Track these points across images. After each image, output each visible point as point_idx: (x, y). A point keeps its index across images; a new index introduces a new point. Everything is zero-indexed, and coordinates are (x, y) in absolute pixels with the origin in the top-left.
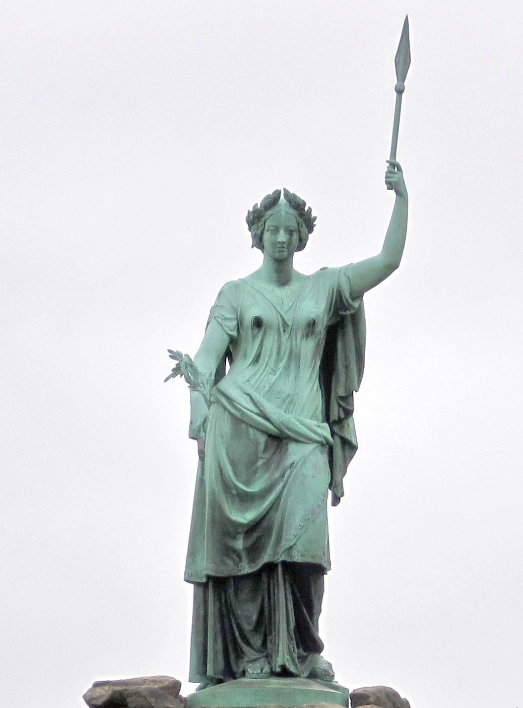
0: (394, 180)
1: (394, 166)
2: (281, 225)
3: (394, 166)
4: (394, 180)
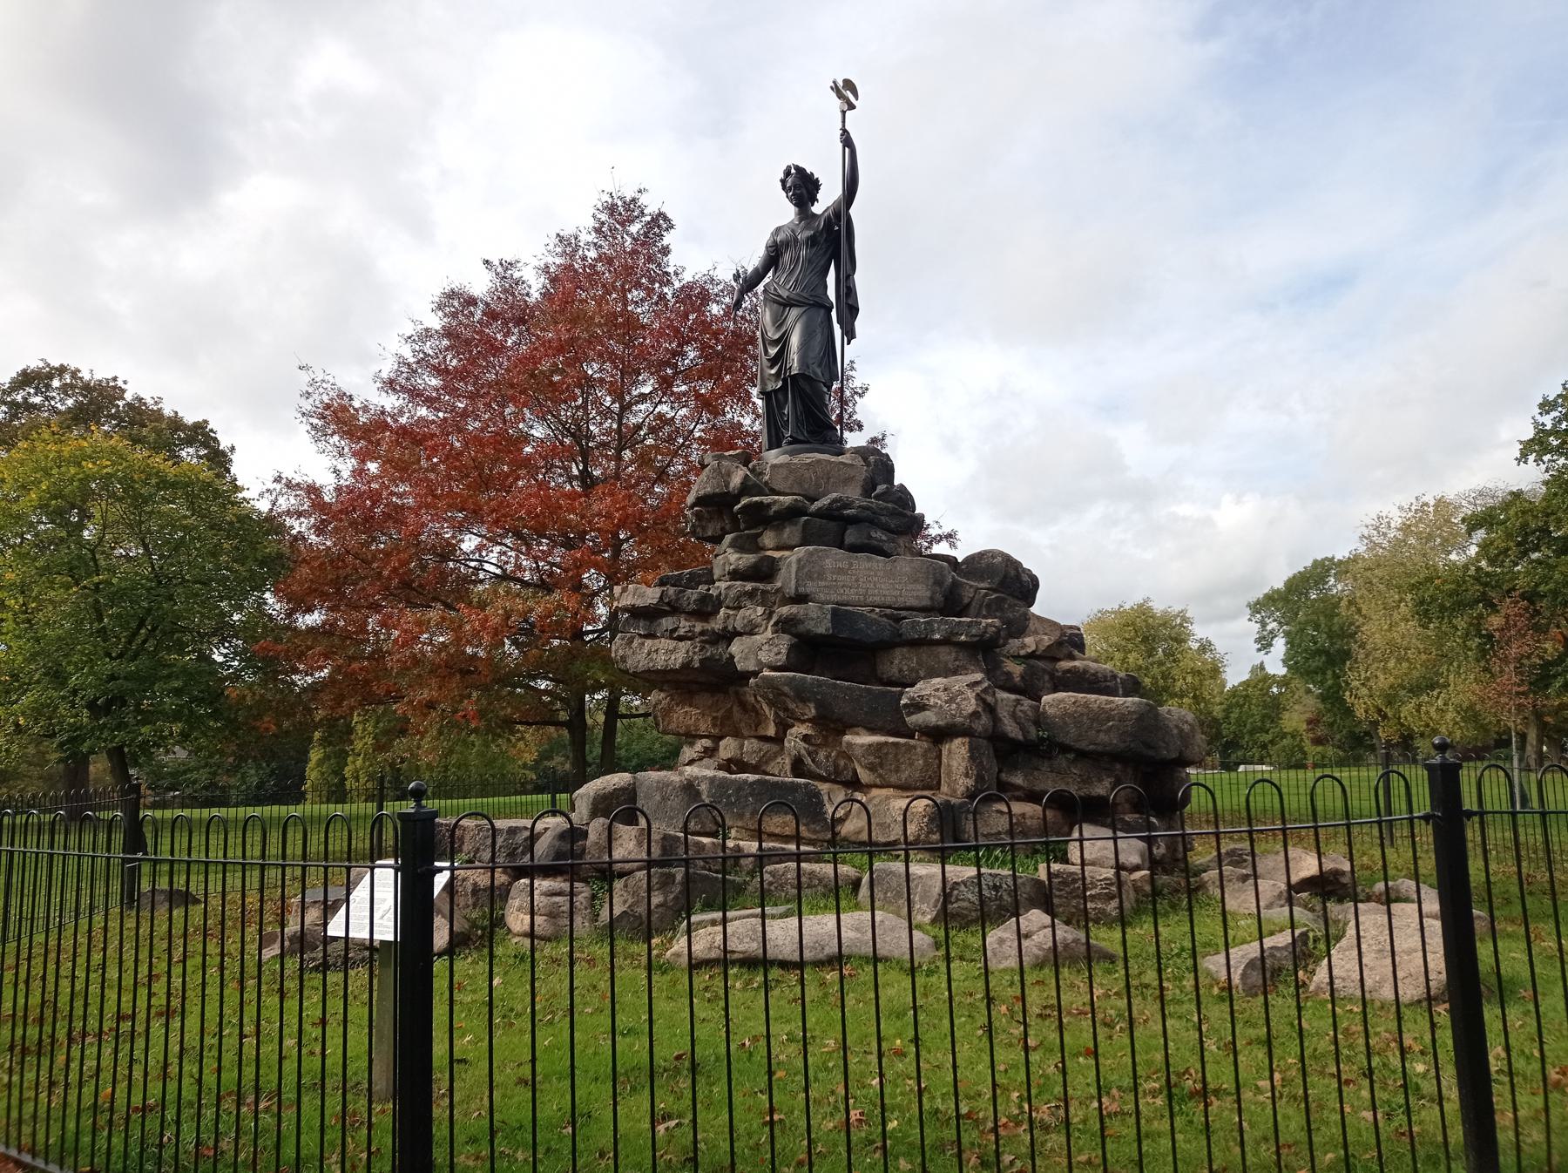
0: (847, 141)
1: (845, 131)
2: (801, 186)
3: (845, 131)
4: (847, 141)
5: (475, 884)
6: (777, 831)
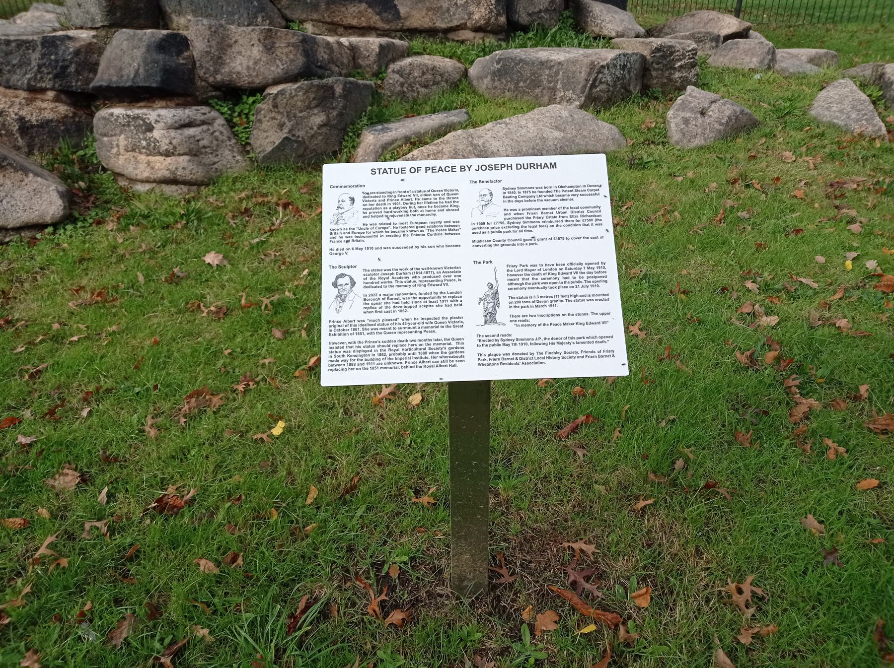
5: (21, 119)
6: (354, 22)
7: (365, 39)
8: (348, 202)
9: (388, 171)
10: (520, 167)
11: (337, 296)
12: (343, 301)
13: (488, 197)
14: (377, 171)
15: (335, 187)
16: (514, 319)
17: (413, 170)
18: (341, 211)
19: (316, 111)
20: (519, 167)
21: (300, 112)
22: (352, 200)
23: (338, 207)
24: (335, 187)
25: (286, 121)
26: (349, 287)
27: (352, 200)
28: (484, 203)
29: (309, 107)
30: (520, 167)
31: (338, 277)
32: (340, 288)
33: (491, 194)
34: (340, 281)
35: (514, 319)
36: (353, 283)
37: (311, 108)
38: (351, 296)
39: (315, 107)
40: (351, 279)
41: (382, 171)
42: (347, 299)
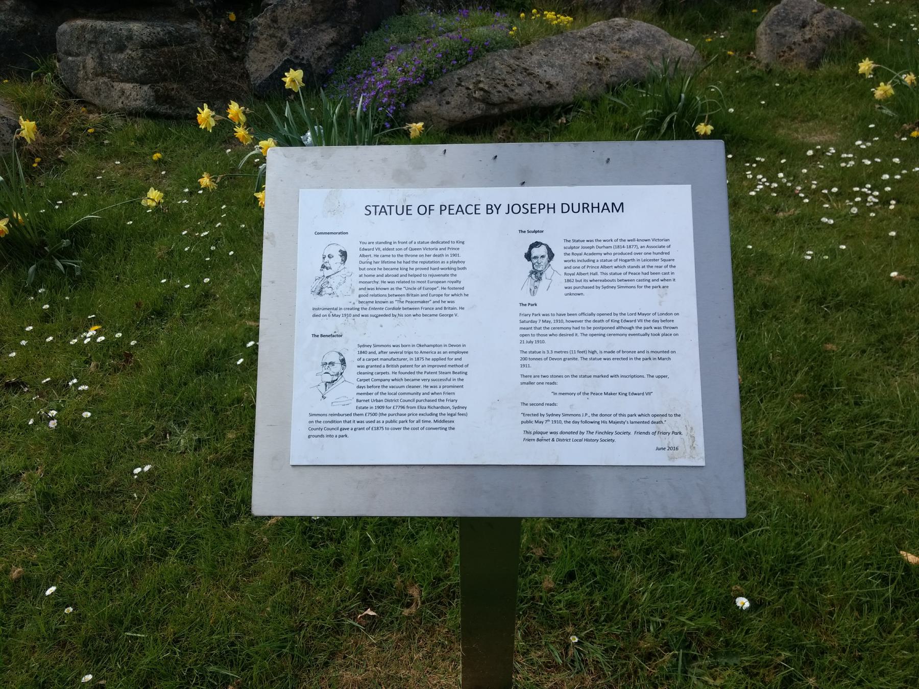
7: (117, 25)
8: (338, 258)
9: (388, 209)
10: (568, 208)
11: (532, 273)
12: (539, 279)
13: (338, 368)
14: (372, 209)
15: (319, 233)
16: (528, 418)
17: (422, 210)
18: (327, 273)
19: (324, 27)
20: (565, 208)
21: (305, 28)
22: (344, 254)
23: (323, 267)
24: (319, 233)
25: (288, 40)
26: (545, 259)
27: (344, 254)
28: (329, 379)
29: (314, 22)
30: (568, 208)
31: (532, 246)
32: (535, 261)
33: (343, 362)
34: (536, 252)
35: (528, 418)
36: (551, 255)
37: (317, 23)
38: (548, 273)
39: (323, 22)
40: (549, 249)
41: (379, 209)
42: (543, 277)
